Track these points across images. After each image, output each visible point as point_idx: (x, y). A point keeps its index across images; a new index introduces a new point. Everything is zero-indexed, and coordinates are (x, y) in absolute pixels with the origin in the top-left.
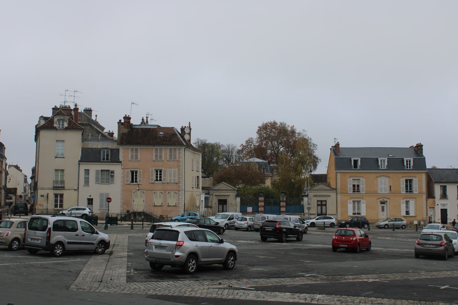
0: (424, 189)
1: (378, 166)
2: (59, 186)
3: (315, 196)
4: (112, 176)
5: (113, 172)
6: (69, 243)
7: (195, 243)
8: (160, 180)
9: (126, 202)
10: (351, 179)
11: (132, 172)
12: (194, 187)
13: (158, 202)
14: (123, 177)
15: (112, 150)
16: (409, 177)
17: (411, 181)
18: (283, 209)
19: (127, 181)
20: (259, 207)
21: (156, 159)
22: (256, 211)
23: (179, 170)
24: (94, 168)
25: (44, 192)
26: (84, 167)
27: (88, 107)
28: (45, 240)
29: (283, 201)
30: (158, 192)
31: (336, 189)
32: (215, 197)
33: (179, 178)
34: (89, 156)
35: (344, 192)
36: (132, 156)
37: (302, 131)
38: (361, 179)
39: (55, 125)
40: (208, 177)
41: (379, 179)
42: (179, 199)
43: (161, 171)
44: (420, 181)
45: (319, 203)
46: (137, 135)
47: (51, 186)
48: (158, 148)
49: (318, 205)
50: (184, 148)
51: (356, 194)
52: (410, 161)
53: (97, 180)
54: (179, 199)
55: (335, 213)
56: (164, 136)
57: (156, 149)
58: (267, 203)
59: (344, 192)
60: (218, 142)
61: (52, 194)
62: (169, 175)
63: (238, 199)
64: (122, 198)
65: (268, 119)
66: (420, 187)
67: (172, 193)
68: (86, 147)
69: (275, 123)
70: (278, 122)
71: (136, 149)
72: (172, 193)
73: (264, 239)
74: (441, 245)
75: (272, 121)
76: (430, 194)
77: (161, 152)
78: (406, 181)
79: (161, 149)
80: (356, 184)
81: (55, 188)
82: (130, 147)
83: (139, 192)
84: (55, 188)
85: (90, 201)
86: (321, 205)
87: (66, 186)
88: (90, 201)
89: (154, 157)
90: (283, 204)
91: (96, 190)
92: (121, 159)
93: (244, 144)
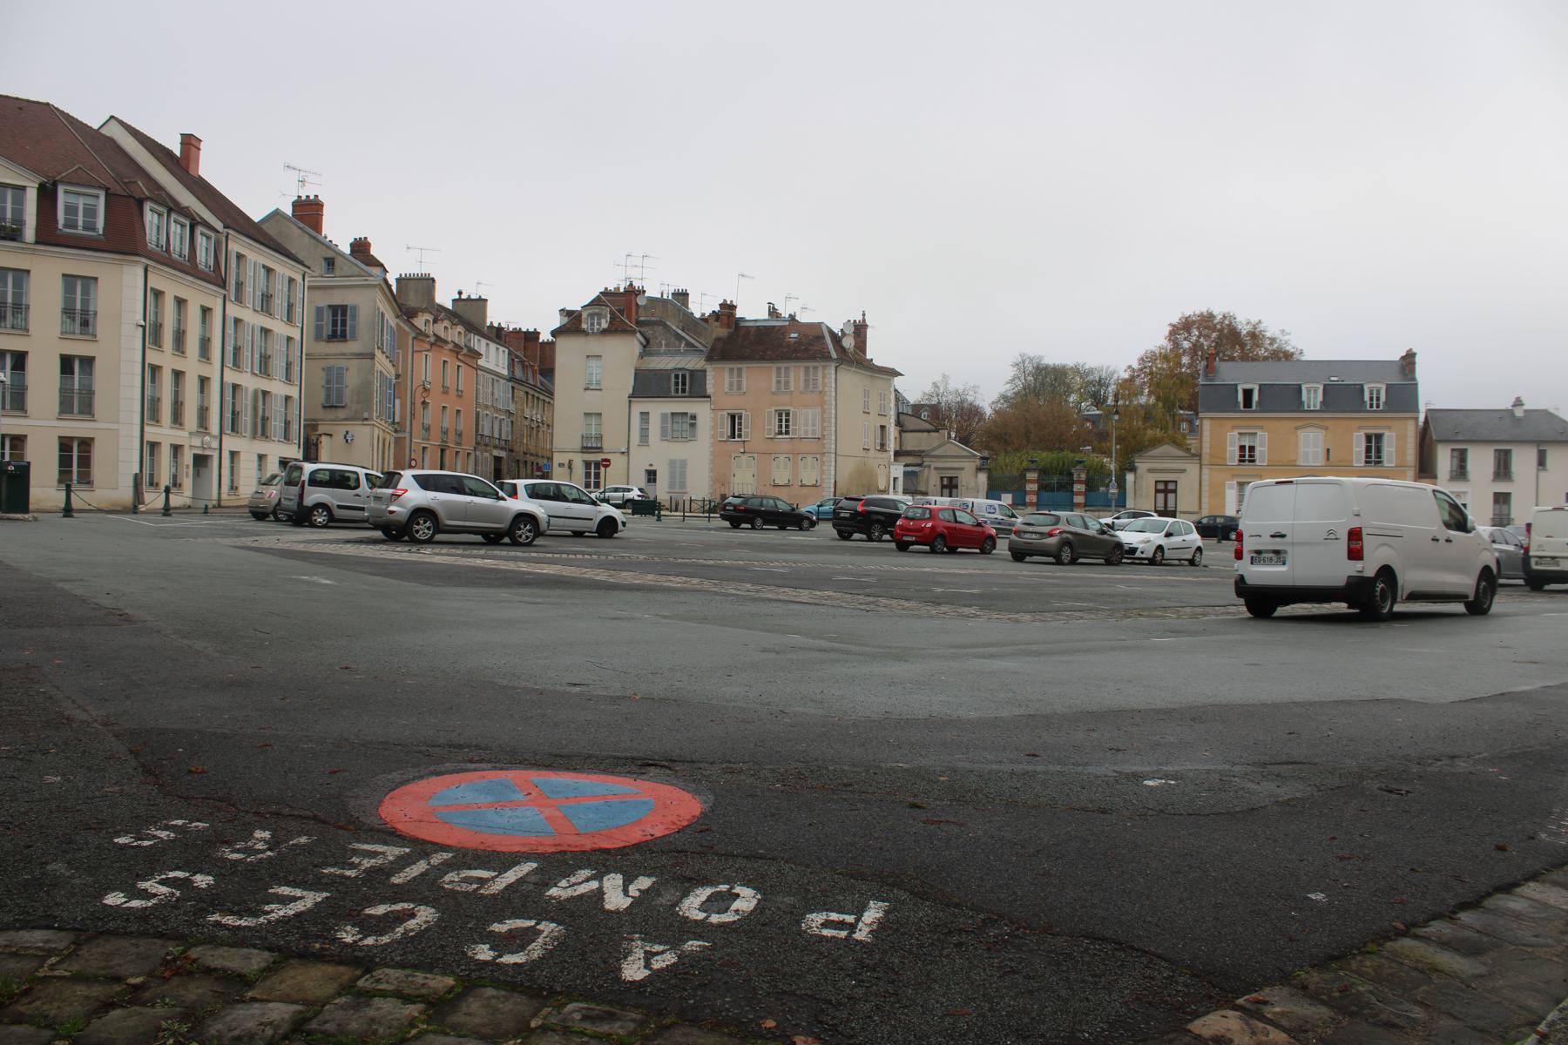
0: (1411, 456)
1: (1301, 403)
2: (590, 446)
3: (1150, 471)
4: (693, 425)
5: (694, 417)
6: (340, 507)
7: (431, 495)
8: (787, 433)
9: (720, 478)
10: (1235, 433)
11: (733, 417)
12: (872, 447)
13: (781, 475)
14: (714, 428)
15: (692, 372)
16: (1374, 427)
17: (1379, 437)
18: (1079, 499)
19: (722, 434)
20: (1026, 493)
21: (778, 388)
22: (1019, 502)
23: (824, 411)
24: (658, 409)
25: (564, 458)
26: (639, 406)
27: (681, 287)
28: (297, 499)
29: (1080, 482)
30: (782, 457)
31: (1200, 456)
32: (934, 473)
33: (823, 429)
34: (647, 385)
35: (1219, 463)
36: (731, 384)
37: (1277, 334)
38: (1259, 433)
39: (584, 326)
40: (937, 431)
41: (1302, 434)
42: (822, 472)
43: (788, 415)
44: (1401, 438)
45: (1161, 486)
46: (741, 341)
47: (578, 446)
48: (783, 365)
49: (1157, 491)
50: (833, 365)
51: (1247, 467)
52: (1378, 392)
53: (664, 435)
54: (822, 472)
55: (1196, 509)
56: (799, 342)
57: (779, 369)
58: (1044, 487)
59: (1219, 463)
60: (1081, 362)
61: (578, 461)
62: (805, 421)
63: (983, 477)
64: (712, 470)
65: (1194, 307)
66: (1401, 452)
67: (809, 458)
68: (643, 367)
69: (1211, 316)
70: (1218, 311)
71: (740, 370)
72: (809, 458)
73: (844, 535)
74: (1050, 535)
75: (1204, 310)
76: (1425, 469)
77: (787, 375)
78: (1369, 438)
79: (787, 369)
80: (1247, 443)
81: (585, 449)
82: (728, 365)
83: (744, 457)
84: (585, 449)
85: (652, 476)
86: (1166, 491)
87: (606, 447)
88: (652, 476)
89: (774, 384)
90: (1078, 487)
91: (659, 453)
92: (710, 390)
93: (1136, 366)
